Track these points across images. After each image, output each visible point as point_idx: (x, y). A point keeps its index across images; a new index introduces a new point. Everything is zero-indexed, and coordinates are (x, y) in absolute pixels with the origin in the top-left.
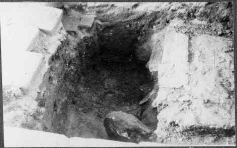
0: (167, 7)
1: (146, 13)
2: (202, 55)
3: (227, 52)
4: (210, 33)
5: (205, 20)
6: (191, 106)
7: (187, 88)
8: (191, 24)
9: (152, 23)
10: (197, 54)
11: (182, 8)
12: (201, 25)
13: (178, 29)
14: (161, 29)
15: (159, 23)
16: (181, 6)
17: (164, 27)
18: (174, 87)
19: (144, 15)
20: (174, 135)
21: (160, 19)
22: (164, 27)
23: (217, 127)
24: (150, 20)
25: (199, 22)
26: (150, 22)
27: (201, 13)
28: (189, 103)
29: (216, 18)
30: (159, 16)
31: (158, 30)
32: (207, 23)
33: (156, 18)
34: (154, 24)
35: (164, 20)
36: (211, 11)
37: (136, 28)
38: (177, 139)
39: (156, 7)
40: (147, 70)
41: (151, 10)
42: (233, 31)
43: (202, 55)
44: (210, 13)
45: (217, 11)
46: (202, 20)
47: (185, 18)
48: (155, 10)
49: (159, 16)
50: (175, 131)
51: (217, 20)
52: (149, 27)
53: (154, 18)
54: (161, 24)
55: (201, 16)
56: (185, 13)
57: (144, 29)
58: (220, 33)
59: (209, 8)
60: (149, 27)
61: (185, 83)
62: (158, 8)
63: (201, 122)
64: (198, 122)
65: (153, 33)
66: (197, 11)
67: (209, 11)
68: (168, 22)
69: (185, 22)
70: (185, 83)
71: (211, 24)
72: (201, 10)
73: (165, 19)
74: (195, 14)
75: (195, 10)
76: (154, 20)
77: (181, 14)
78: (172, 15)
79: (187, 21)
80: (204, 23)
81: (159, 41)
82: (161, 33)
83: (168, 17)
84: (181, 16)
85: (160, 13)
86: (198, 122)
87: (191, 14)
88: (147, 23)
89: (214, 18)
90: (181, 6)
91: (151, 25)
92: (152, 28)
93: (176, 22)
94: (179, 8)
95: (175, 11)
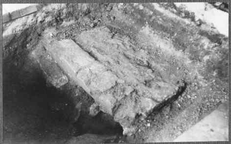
0: (33, 20)
1: (15, 35)
2: (100, 50)
3: (112, 38)
4: (84, 29)
5: (72, 19)
6: (139, 93)
7: (119, 81)
8: (63, 28)
9: (25, 42)
10: (94, 51)
11: (47, 16)
12: (72, 25)
13: (57, 37)
14: (35, 45)
15: (31, 40)
16: (45, 15)
17: (38, 42)
18: (111, 86)
19: (14, 38)
20: (141, 125)
21: (31, 35)
22: (38, 42)
23: (170, 97)
24: (22, 41)
25: (69, 23)
26: (23, 41)
27: (66, 15)
28: (135, 91)
29: (80, 14)
30: (29, 33)
31: (33, 47)
32: (75, 21)
33: (27, 37)
34: (27, 43)
35: (36, 35)
36: (73, 9)
37: (10, 54)
38: (145, 126)
39: (22, 25)
40: (53, 88)
41: (20, 30)
42: (100, 19)
43: (100, 50)
44: (73, 11)
45: (78, 7)
46: (70, 20)
47: (55, 24)
48: (24, 29)
49: (29, 33)
50: (140, 121)
51: (81, 15)
52: (23, 48)
53: (25, 37)
54: (33, 40)
55: (66, 17)
56: (53, 20)
57: (18, 52)
58: (92, 25)
59: (70, 7)
60: (23, 48)
61: (114, 78)
62: (25, 25)
63: (159, 100)
64: (156, 101)
65: (29, 52)
66: (61, 14)
67: (72, 9)
68: (40, 35)
69: (57, 28)
70: (114, 78)
71: (79, 21)
72: (65, 11)
73: (36, 33)
74: (62, 17)
75: (60, 14)
76: (26, 39)
77: (50, 22)
78: (42, 26)
79: (58, 27)
80: (72, 22)
81: (41, 56)
82: (40, 46)
83: (39, 30)
84: (50, 24)
85: (30, 29)
86: (156, 101)
87: (58, 18)
88: (20, 44)
89: (78, 14)
90: (45, 15)
91: (24, 46)
92: (26, 47)
93: (49, 33)
94: (45, 17)
95: (44, 21)
